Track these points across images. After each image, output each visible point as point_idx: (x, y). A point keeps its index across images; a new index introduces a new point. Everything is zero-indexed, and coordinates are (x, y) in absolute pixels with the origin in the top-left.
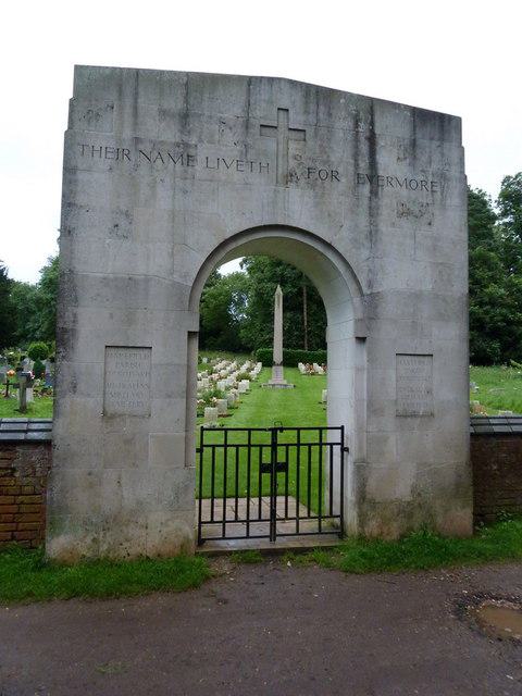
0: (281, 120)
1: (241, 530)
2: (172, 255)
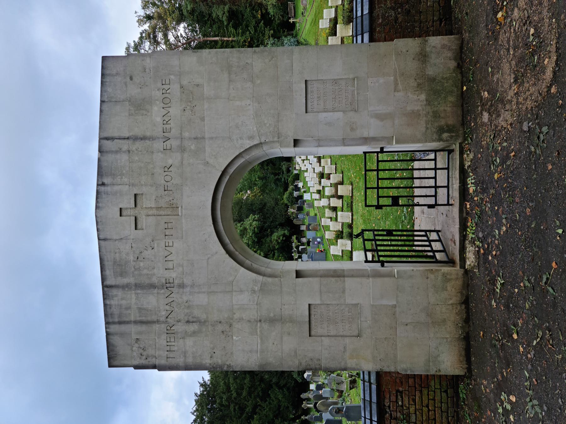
0: (129, 213)
1: (442, 193)
2: (241, 291)
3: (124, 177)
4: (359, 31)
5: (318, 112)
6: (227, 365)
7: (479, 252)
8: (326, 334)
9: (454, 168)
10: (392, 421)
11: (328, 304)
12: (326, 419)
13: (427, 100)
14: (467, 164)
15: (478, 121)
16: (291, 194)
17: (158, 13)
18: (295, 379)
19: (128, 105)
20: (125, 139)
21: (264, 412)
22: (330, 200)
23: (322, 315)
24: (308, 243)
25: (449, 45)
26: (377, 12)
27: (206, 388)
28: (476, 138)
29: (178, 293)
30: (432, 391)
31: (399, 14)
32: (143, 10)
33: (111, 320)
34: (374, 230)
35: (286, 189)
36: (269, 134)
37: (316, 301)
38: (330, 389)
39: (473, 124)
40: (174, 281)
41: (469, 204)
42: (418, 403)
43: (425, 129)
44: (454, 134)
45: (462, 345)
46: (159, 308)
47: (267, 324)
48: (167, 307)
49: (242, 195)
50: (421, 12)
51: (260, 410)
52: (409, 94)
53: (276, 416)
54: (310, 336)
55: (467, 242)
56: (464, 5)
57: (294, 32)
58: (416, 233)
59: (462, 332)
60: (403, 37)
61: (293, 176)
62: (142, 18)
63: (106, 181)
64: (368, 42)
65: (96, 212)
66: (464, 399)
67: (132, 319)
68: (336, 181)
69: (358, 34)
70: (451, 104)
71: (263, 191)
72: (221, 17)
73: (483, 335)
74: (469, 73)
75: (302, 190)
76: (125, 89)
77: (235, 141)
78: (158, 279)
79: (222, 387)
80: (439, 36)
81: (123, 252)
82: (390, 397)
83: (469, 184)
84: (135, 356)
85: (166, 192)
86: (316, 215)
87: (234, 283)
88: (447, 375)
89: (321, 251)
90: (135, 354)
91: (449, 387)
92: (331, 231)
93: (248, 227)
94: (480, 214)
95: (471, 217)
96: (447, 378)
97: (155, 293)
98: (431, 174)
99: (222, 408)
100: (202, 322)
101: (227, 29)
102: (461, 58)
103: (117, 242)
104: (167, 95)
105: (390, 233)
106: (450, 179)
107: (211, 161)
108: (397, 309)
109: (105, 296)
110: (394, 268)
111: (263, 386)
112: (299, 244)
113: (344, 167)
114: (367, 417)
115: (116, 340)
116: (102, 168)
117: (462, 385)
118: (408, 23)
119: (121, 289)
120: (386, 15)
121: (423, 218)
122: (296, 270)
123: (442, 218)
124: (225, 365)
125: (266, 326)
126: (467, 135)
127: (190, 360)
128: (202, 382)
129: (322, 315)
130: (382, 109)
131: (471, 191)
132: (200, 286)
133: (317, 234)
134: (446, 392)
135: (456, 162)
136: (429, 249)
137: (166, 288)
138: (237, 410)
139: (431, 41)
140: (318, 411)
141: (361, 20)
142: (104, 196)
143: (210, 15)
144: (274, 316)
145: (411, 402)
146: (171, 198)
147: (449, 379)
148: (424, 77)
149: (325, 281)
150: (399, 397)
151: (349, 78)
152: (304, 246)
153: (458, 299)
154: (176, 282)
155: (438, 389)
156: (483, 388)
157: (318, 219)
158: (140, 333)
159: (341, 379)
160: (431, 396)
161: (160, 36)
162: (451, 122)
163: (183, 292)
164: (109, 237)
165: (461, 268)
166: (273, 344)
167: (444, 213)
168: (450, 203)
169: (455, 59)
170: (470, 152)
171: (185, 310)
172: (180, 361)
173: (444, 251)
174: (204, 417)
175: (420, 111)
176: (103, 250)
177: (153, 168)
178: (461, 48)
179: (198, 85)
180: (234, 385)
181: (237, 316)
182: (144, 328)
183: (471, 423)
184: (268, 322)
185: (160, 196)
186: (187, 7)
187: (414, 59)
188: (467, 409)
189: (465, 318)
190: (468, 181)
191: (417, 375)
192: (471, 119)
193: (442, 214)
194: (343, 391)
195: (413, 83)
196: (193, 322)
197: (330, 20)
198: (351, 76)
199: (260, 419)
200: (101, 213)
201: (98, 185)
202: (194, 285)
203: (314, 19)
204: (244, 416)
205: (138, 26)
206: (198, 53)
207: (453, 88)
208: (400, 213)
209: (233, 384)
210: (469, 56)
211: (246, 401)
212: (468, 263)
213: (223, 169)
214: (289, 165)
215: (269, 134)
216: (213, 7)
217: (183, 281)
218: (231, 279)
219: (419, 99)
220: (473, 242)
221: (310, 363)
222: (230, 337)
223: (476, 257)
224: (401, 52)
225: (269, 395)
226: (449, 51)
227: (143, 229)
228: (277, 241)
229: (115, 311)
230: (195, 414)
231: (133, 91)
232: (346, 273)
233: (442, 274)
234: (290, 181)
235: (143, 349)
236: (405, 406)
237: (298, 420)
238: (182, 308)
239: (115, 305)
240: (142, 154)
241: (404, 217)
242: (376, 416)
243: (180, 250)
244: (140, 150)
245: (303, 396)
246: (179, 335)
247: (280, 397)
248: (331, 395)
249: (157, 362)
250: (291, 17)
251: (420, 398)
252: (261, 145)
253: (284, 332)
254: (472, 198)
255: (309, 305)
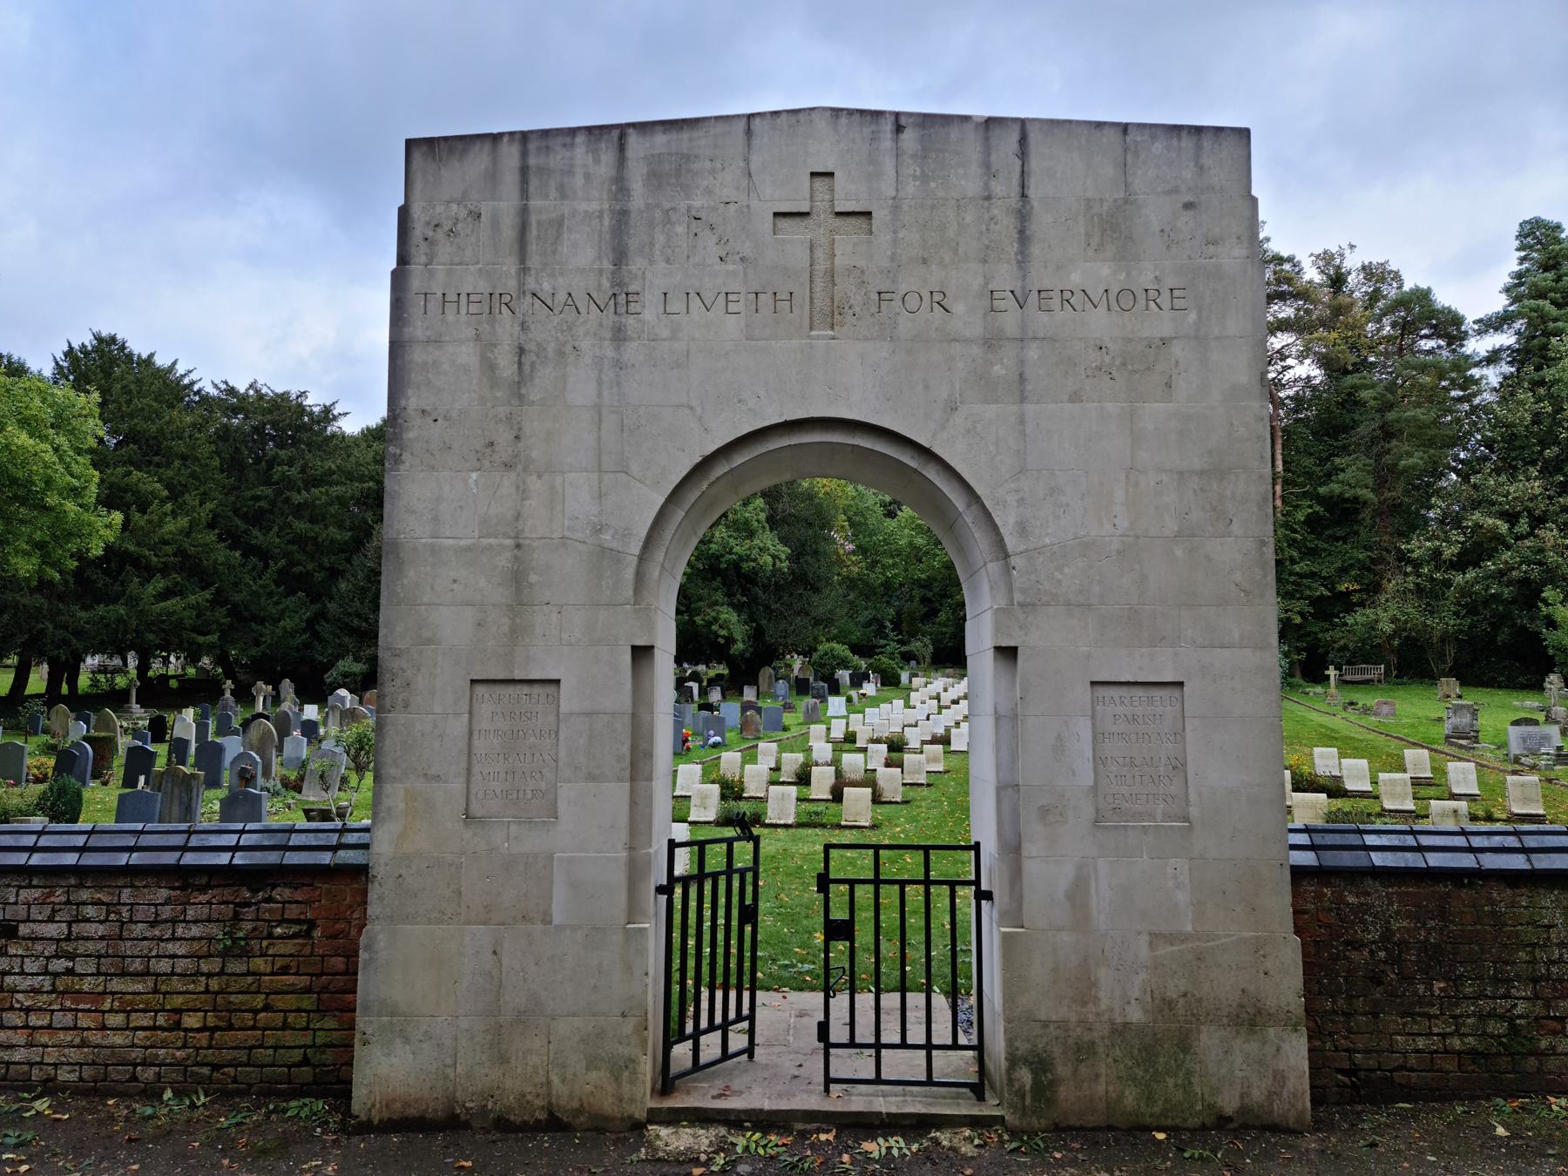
0: (819, 196)
1: (863, 1065)
3: (918, 183)
4: (1323, 837)
5: (1093, 717)
6: (401, 455)
7: (696, 1162)
8: (476, 727)
9: (930, 1100)
10: (231, 906)
11: (557, 733)
12: (226, 745)
13: (1125, 1024)
14: (944, 1137)
15: (1067, 1171)
16: (844, 664)
17: (1352, 304)
18: (333, 665)
19: (1116, 196)
20: (1023, 187)
21: (248, 579)
22: (829, 765)
23: (529, 715)
24: (707, 707)
25: (1285, 1094)
26: (1377, 891)
27: (318, 423)
28: (1019, 1164)
29: (601, 325)
30: (308, 1023)
31: (1372, 952)
32: (1359, 265)
33: (532, 146)
34: (755, 870)
35: (856, 649)
36: (1033, 577)
37: (568, 699)
38: (304, 757)
39: (1058, 1155)
40: (632, 317)
41: (831, 1139)
42: (278, 981)
43: (1043, 1017)
44: (1028, 1101)
45: (435, 1111)
46: (561, 274)
47: (510, 565)
48: (561, 297)
49: (843, 527)
50: (1376, 1015)
51: (254, 568)
52: (1143, 976)
53: (235, 611)
54: (473, 682)
55: (723, 1131)
56: (1396, 1137)
57: (1298, 680)
58: (746, 995)
59: (471, 1108)
60: (1305, 963)
61: (893, 668)
62: (1338, 261)
63: (909, 136)
64: (1292, 862)
65: (824, 109)
66: (285, 1111)
67: (534, 203)
68: (881, 783)
69: (1312, 835)
70: (1114, 1095)
71: (851, 583)
72: (1341, 476)
73: (463, 1167)
74: (1205, 1149)
75: (853, 693)
76: (1159, 189)
77: (1013, 486)
78: (640, 273)
79: (319, 463)
80: (1310, 1068)
81: (715, 178)
82: (297, 902)
83: (887, 1140)
84: (434, 208)
85: (876, 297)
86: (785, 729)
87: (622, 477)
88: (352, 1065)
89: (686, 741)
90: (440, 209)
91: (318, 1070)
92: (742, 767)
93: (756, 542)
94: (803, 1169)
95: (793, 1143)
96: (342, 1065)
97: (601, 264)
98: (916, 1035)
99: (263, 463)
100: (519, 388)
101: (1305, 495)
102: (1246, 1127)
103: (742, 164)
104: (1142, 301)
105: (749, 915)
106: (899, 1088)
107: (959, 419)
108: (539, 927)
109: (597, 132)
110: (653, 922)
111: (319, 576)
112: (705, 684)
113: (920, 807)
114: (244, 836)
115: (478, 161)
116: (943, 126)
117: (323, 1108)
118: (1346, 979)
119: (613, 172)
120: (1367, 917)
121: (787, 1014)
122: (653, 647)
123: (788, 1065)
124: (401, 449)
125: (504, 561)
126: (1025, 1138)
127: (417, 355)
128: (336, 412)
129: (529, 715)
130: (1101, 896)
131: (867, 1146)
132: (618, 384)
133: (731, 731)
134: (305, 1061)
135: (949, 1105)
136: (704, 1024)
137: (615, 294)
138: (257, 504)
139: (1295, 1043)
140: (246, 724)
141: (1353, 843)
142: (867, 130)
143: (1345, 449)
144: (531, 585)
145: (279, 963)
146: (857, 309)
147: (339, 1070)
148: (1194, 1019)
149: (623, 727)
150: (295, 929)
151: (1187, 805)
152: (700, 695)
153: (563, 1102)
154: (631, 321)
155: (314, 1038)
156: (313, 1163)
157: (773, 735)
158: (495, 224)
159: (334, 786)
160: (295, 1017)
161: (1286, 311)
162: (1065, 1093)
163: (601, 339)
164: (755, 142)
165: (651, 1111)
166: (455, 581)
167: (802, 1069)
168: (832, 1087)
169: (1243, 1110)
170: (977, 1146)
171: (553, 344)
172: (417, 329)
173: (697, 1066)
174: (241, 416)
175: (1094, 1004)
176: (720, 128)
177: (941, 263)
178: (1275, 1128)
179: (1170, 387)
180: (324, 498)
181: (534, 483)
182: (509, 233)
183: (218, 1129)
184: (515, 567)
185: (865, 279)
186: (1366, 387)
187: (1243, 991)
188: (255, 1118)
189: (508, 1120)
190: (895, 1138)
191: (357, 980)
192: (1071, 1150)
193: (800, 1066)
194: (300, 792)
195: (1175, 987)
196: (520, 363)
197: (1338, 779)
198: (1194, 812)
199: (230, 567)
200: (821, 123)
201: (897, 115)
202: (621, 368)
203: (1337, 735)
204: (239, 523)
205: (1312, 255)
206: (1260, 386)
207: (1160, 1103)
208: (797, 953)
209: (327, 493)
210: (1252, 1151)
211: (281, 529)
212: (664, 1132)
213: (937, 450)
214: (924, 658)
215: (1033, 577)
216: (1367, 456)
217: (632, 339)
218: (635, 468)
219: (1129, 1003)
220: (722, 1147)
221: (398, 682)
222: (478, 465)
223: (681, 1153)
224: (1264, 956)
225: (291, 592)
226: (1266, 1093)
227: (775, 234)
228: (716, 620)
229: (557, 159)
230: (251, 392)
231: (1154, 212)
232: (642, 784)
233: (633, 1057)
234: (879, 660)
235: (451, 231)
236: (269, 944)
237: (220, 670)
238: (559, 334)
239: (571, 159)
240: (981, 232)
241: (787, 962)
242: (247, 862)
243: (716, 333)
244: (992, 226)
245: (287, 686)
246: (485, 325)
247: (288, 623)
248: (290, 760)
249: (416, 268)
250: (1341, 670)
251: (291, 989)
252: (1002, 555)
253: (485, 612)
254: (847, 1149)
255: (558, 682)
